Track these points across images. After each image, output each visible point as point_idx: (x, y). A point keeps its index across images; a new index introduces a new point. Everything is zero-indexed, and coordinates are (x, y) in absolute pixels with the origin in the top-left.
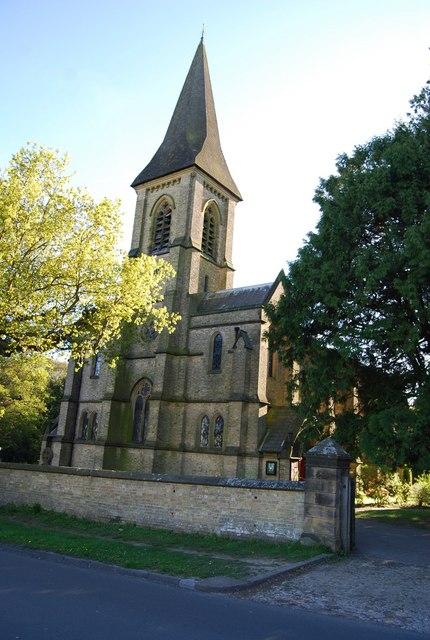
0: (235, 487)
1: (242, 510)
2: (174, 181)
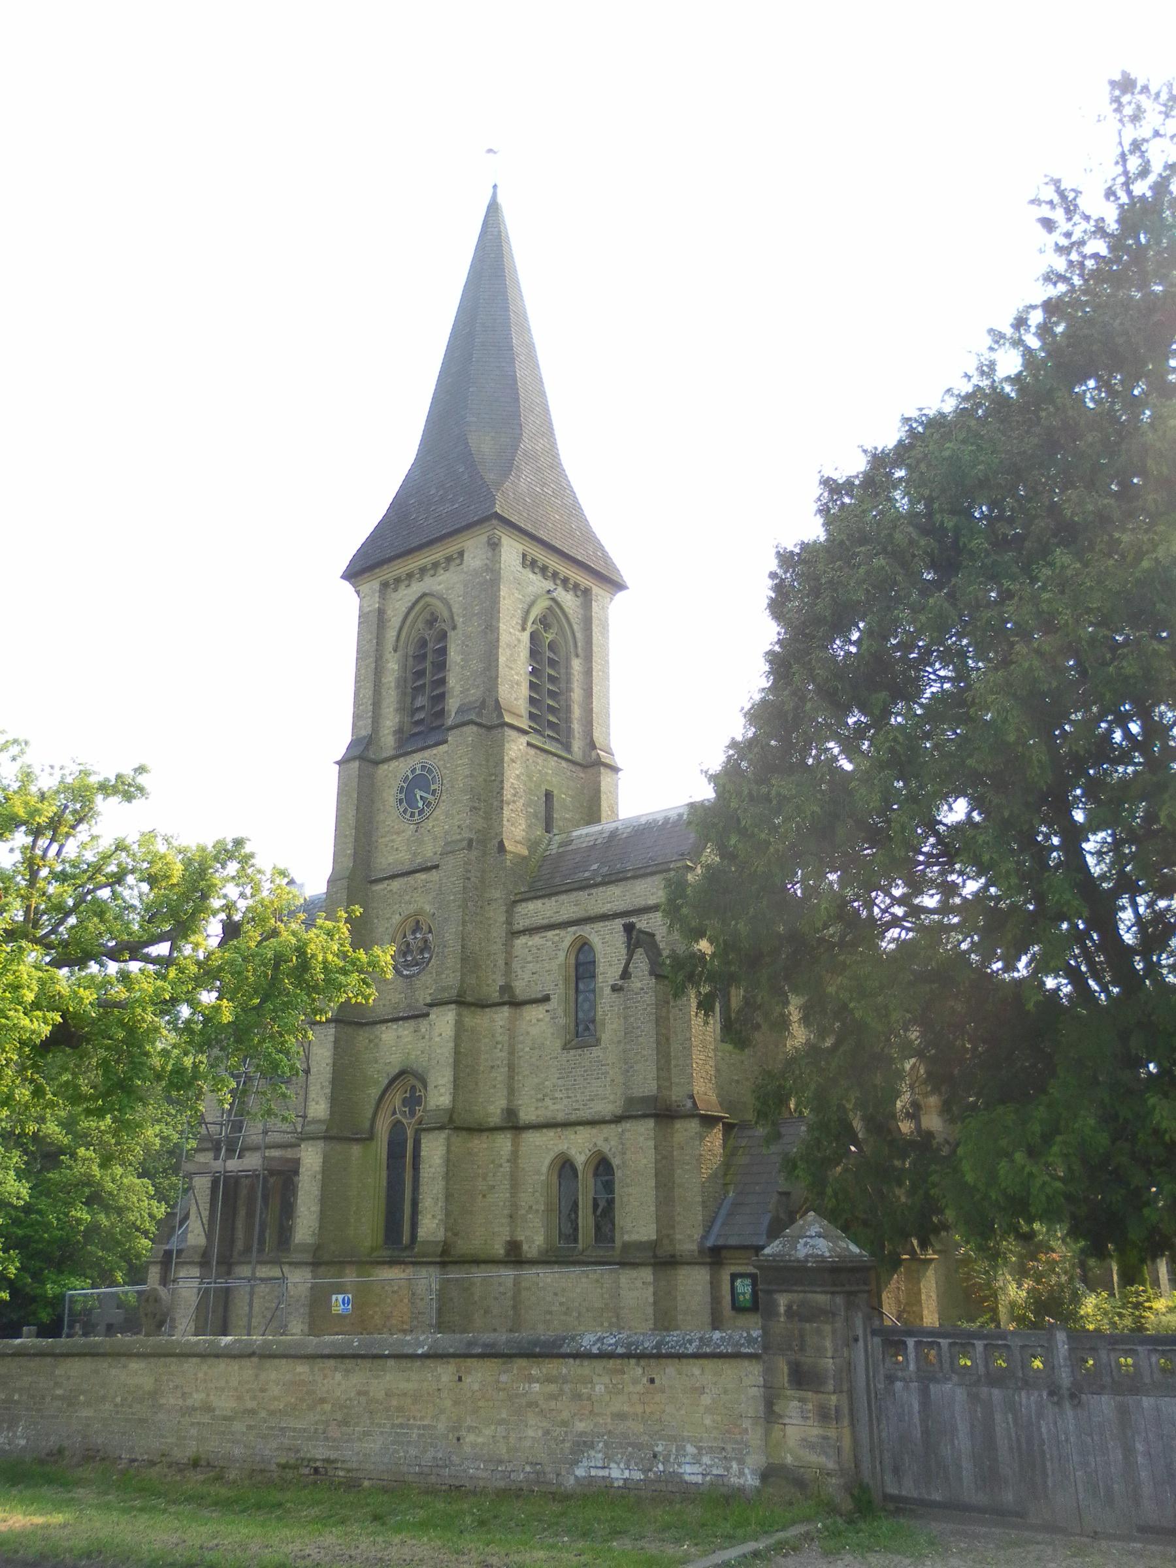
0: (603, 1356)
1: (621, 1416)
2: (449, 559)
